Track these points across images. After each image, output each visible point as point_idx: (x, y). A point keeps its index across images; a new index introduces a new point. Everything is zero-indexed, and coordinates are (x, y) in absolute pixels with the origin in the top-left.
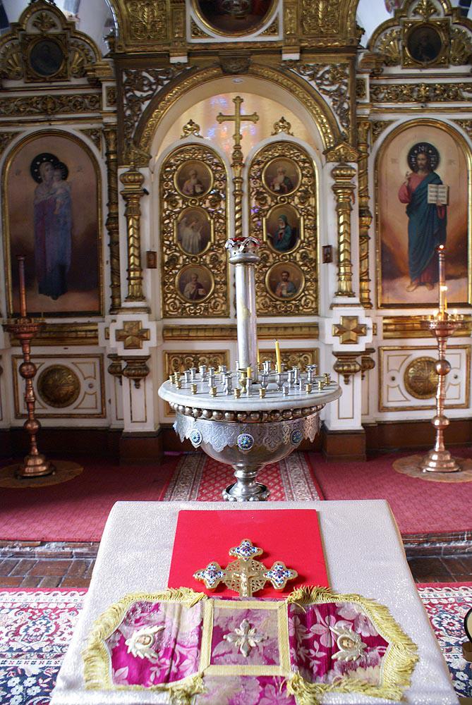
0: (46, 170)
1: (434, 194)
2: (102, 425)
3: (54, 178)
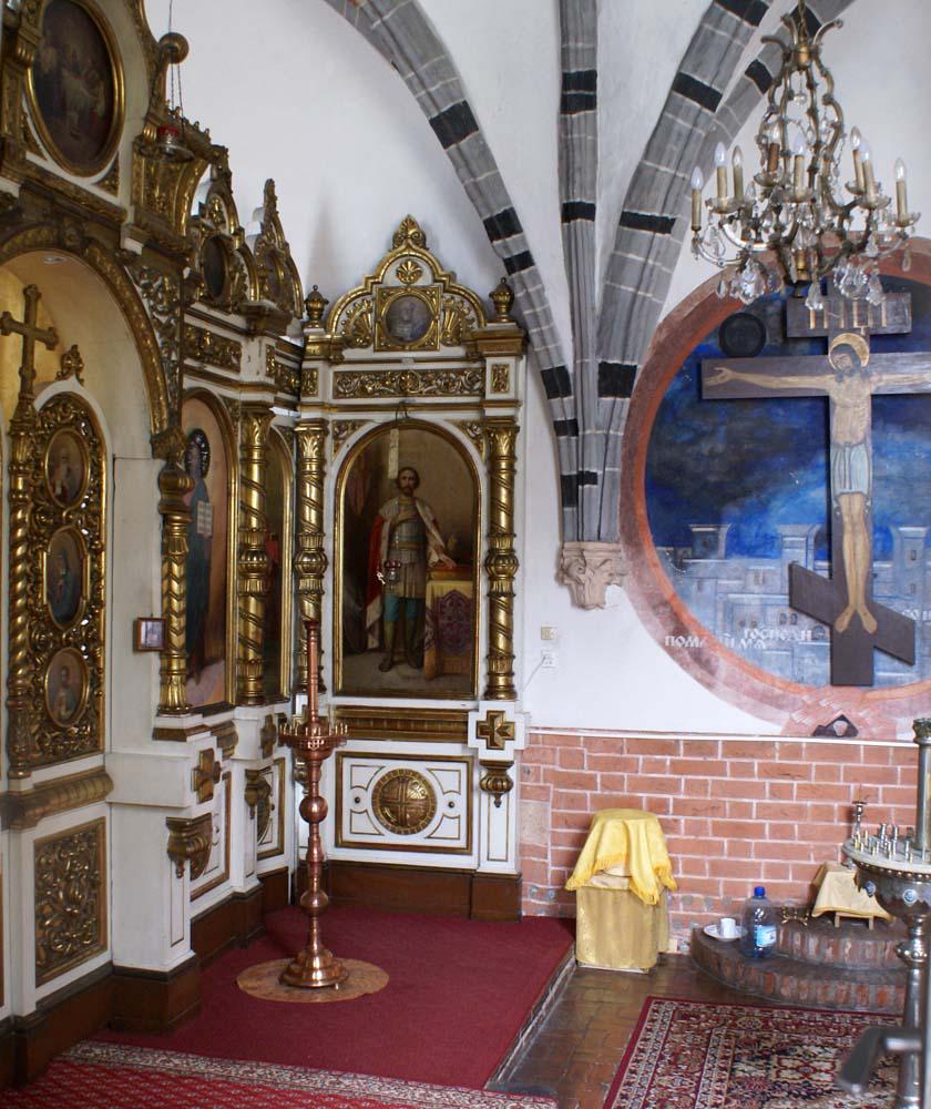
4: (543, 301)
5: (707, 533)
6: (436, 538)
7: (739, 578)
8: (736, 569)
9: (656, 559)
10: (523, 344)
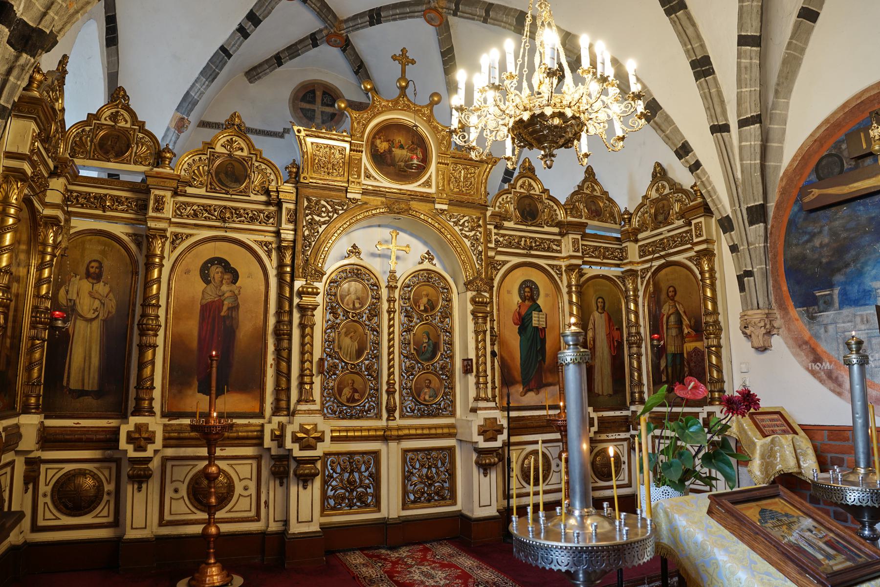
0: (216, 272)
1: (537, 319)
2: (553, 500)
3: (224, 282)
4: (710, 183)
5: (826, 295)
6: (686, 321)
7: (851, 321)
8: (848, 316)
9: (797, 316)
10: (708, 211)
